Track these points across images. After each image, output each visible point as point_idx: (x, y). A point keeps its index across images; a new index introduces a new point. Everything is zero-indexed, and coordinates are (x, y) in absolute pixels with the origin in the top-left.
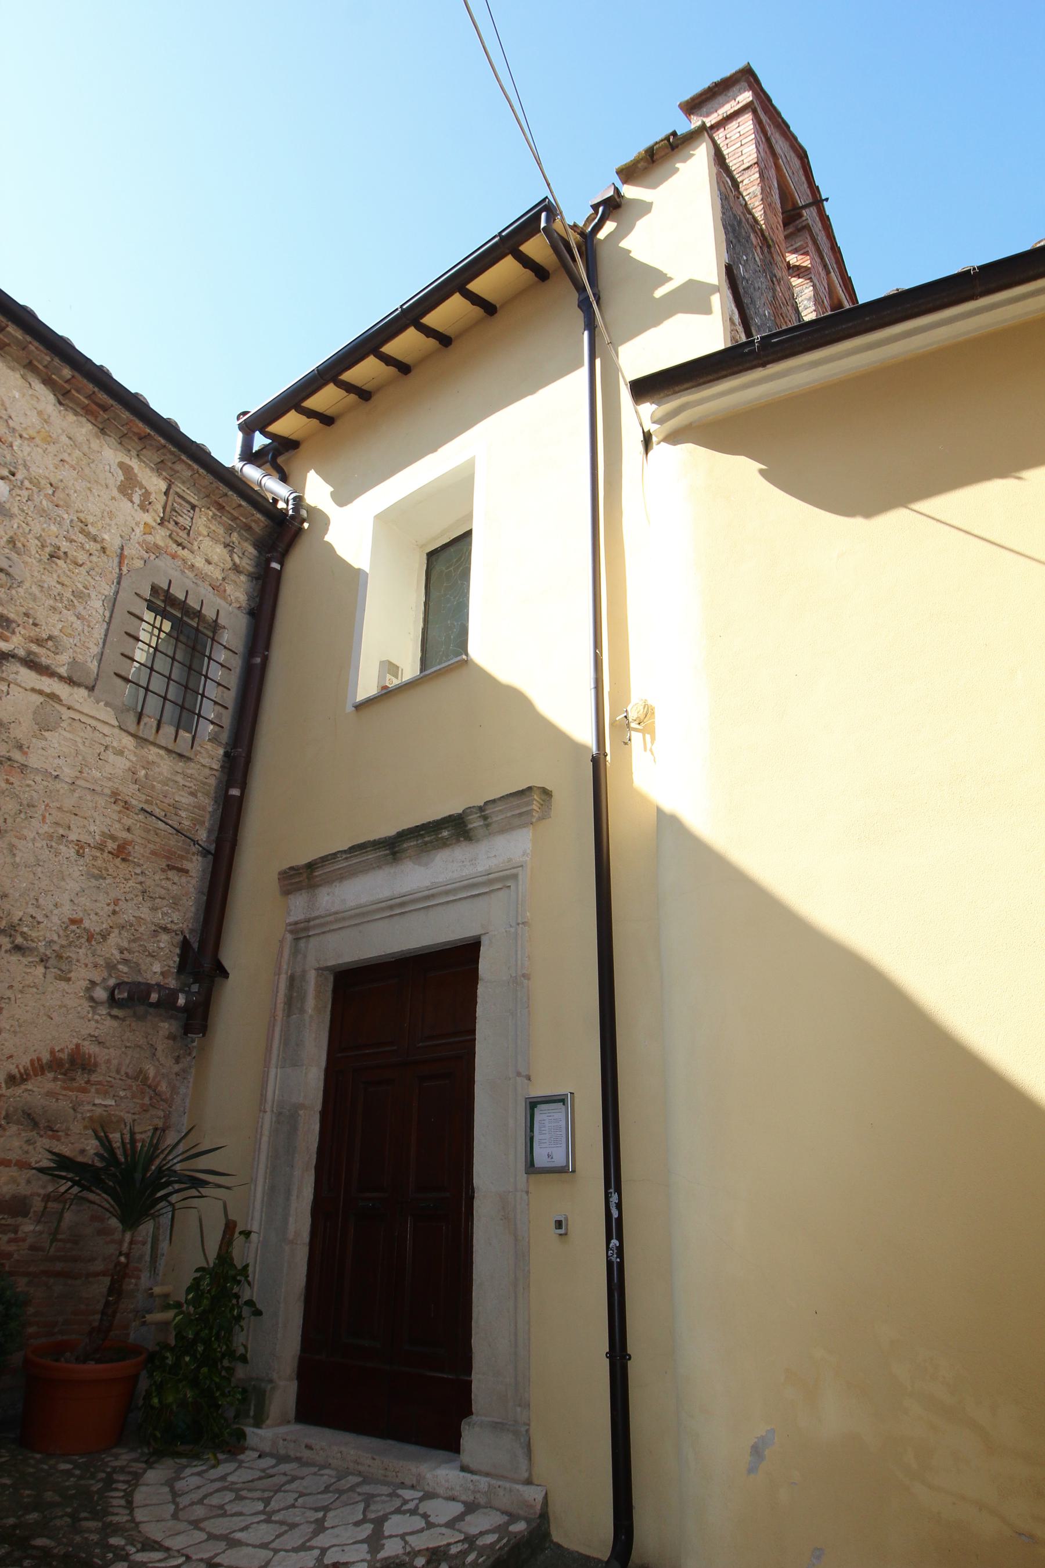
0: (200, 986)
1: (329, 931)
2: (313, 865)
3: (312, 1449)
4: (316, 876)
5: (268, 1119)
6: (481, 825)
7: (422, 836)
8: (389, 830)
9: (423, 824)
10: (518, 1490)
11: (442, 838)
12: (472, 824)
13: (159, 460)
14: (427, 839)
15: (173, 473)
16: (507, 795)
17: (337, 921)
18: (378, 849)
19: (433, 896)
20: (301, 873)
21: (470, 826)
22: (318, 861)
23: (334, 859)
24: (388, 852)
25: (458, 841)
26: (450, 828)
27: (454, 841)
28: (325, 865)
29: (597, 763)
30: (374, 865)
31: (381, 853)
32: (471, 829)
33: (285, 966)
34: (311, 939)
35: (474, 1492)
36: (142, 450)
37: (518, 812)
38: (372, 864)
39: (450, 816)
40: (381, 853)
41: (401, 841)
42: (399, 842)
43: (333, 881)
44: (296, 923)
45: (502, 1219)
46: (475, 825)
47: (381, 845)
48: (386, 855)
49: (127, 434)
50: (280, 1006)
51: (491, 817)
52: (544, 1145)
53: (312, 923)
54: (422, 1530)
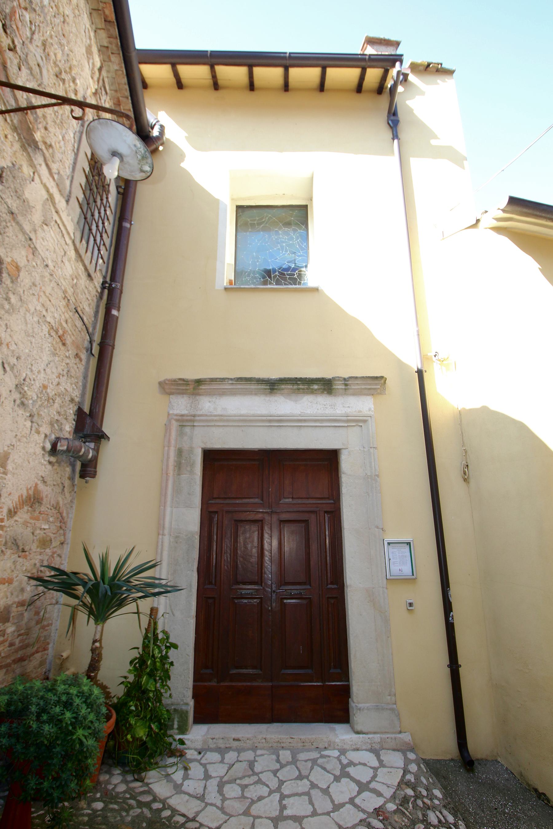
0: (95, 445)
1: (215, 426)
2: (203, 381)
3: (240, 740)
4: (201, 389)
5: (166, 539)
6: (342, 388)
7: (298, 384)
8: (274, 375)
9: (301, 378)
10: (400, 738)
11: (312, 389)
12: (336, 385)
13: (106, 45)
14: (301, 387)
15: (107, 60)
16: (366, 377)
17: (221, 421)
18: (261, 384)
19: (305, 421)
20: (189, 384)
21: (334, 387)
22: (207, 380)
23: (222, 381)
24: (268, 387)
25: (322, 393)
26: (320, 385)
27: (320, 392)
28: (211, 384)
29: (420, 373)
30: (253, 393)
31: (262, 387)
32: (334, 389)
33: (173, 442)
34: (196, 428)
35: (371, 743)
36: (100, 29)
37: (369, 387)
38: (252, 392)
39: (323, 378)
40: (262, 387)
41: (281, 383)
42: (279, 383)
43: (214, 395)
44: (182, 415)
45: (368, 602)
46: (339, 387)
47: (264, 382)
48: (266, 389)
49: (100, 10)
50: (171, 468)
51: (350, 386)
52: (396, 565)
53: (197, 418)
54: (210, 763)
